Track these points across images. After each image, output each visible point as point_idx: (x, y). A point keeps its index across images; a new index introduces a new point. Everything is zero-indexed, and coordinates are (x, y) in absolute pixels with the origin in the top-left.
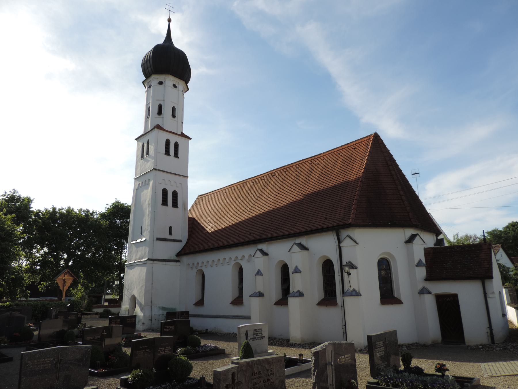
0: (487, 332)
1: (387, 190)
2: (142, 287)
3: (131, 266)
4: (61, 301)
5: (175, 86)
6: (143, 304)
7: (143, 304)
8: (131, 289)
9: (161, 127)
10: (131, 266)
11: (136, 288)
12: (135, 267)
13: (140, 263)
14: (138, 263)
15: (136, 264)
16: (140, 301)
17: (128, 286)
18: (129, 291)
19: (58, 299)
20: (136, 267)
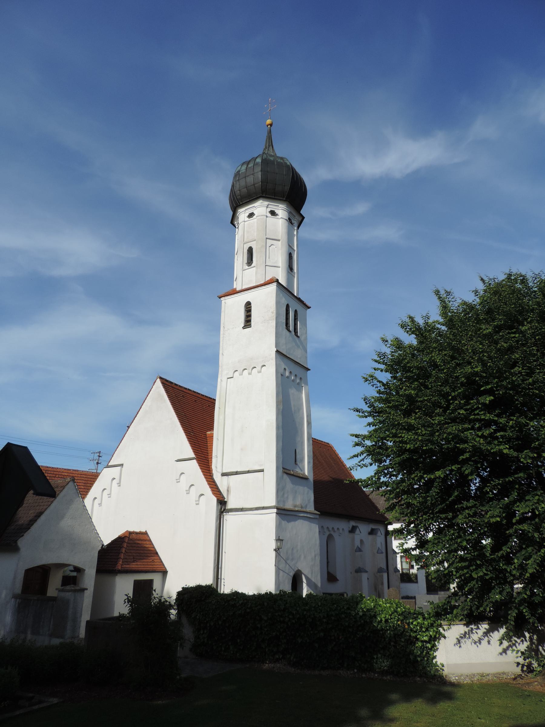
0: (186, 585)
1: (148, 553)
2: (315, 556)
3: (289, 515)
4: (500, 448)
5: (273, 213)
6: (319, 585)
7: (319, 585)
8: (292, 559)
9: (31, 521)
10: (289, 515)
11: (305, 557)
12: (296, 520)
13: (308, 515)
14: (305, 515)
15: (302, 515)
16: (313, 580)
17: (287, 553)
18: (288, 562)
19: (420, 343)
20: (299, 519)
